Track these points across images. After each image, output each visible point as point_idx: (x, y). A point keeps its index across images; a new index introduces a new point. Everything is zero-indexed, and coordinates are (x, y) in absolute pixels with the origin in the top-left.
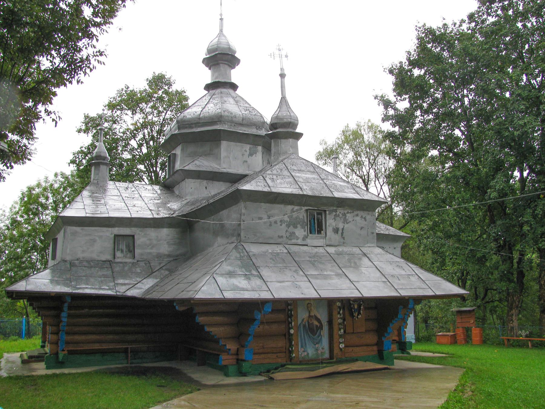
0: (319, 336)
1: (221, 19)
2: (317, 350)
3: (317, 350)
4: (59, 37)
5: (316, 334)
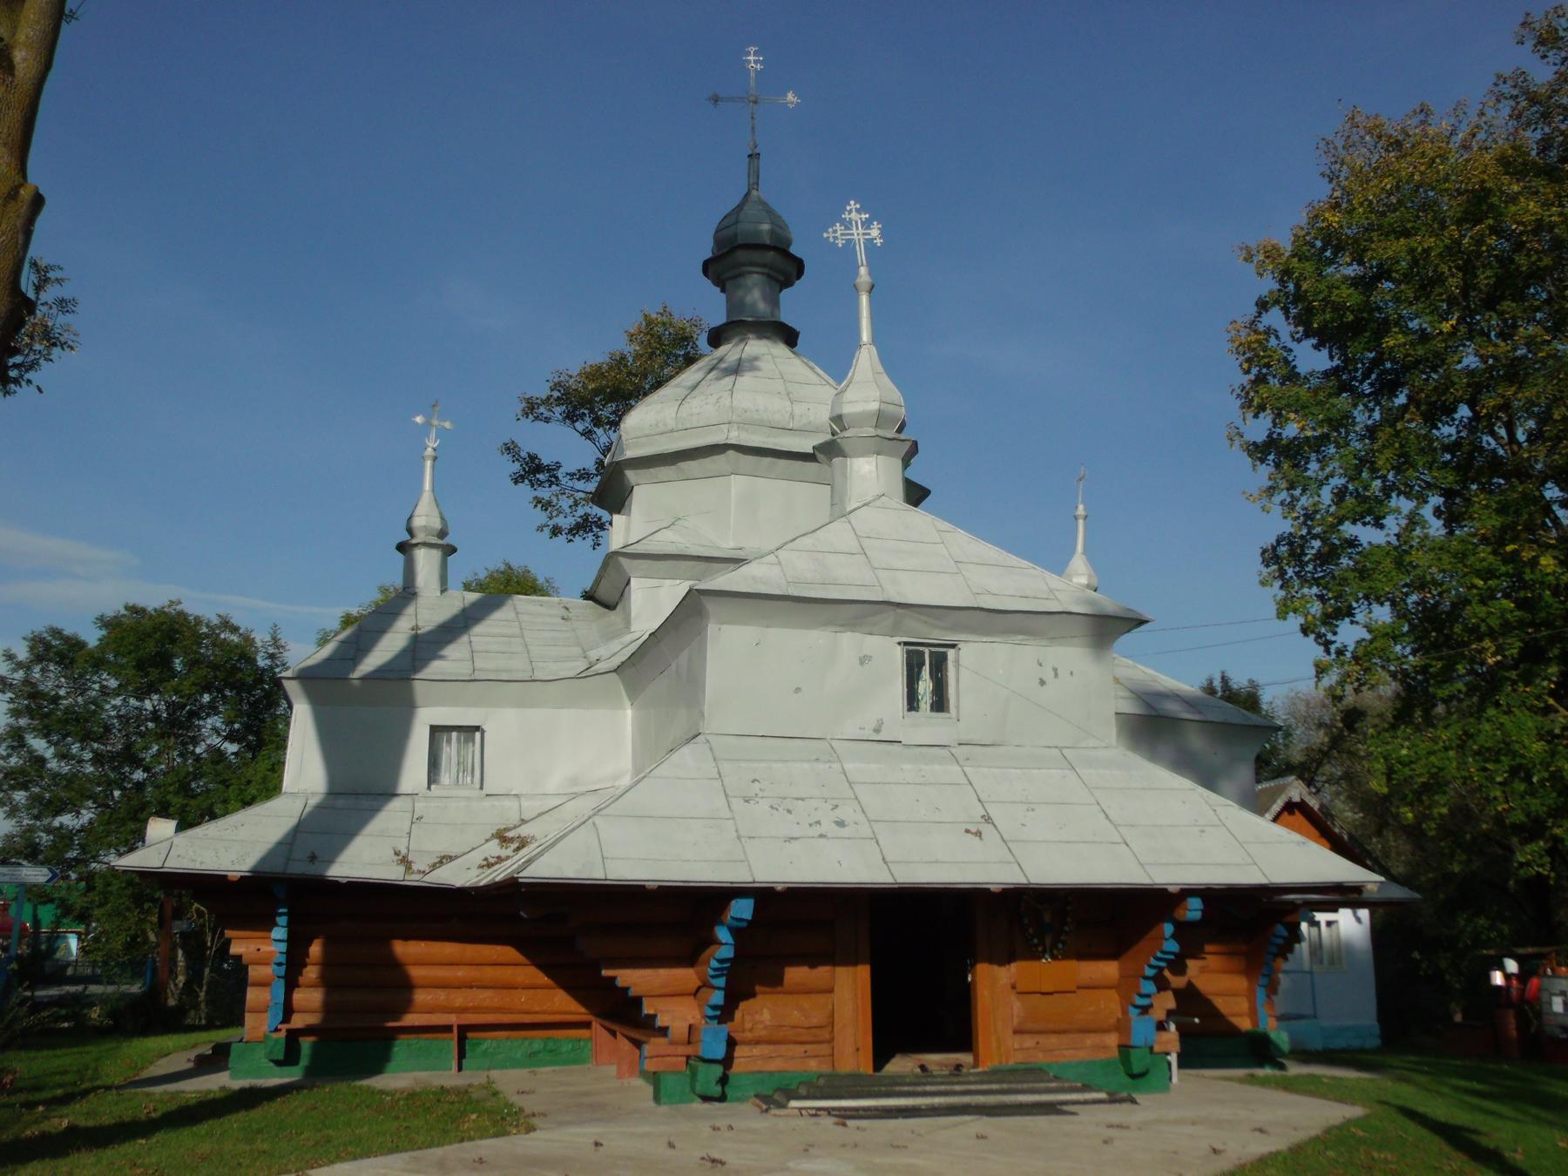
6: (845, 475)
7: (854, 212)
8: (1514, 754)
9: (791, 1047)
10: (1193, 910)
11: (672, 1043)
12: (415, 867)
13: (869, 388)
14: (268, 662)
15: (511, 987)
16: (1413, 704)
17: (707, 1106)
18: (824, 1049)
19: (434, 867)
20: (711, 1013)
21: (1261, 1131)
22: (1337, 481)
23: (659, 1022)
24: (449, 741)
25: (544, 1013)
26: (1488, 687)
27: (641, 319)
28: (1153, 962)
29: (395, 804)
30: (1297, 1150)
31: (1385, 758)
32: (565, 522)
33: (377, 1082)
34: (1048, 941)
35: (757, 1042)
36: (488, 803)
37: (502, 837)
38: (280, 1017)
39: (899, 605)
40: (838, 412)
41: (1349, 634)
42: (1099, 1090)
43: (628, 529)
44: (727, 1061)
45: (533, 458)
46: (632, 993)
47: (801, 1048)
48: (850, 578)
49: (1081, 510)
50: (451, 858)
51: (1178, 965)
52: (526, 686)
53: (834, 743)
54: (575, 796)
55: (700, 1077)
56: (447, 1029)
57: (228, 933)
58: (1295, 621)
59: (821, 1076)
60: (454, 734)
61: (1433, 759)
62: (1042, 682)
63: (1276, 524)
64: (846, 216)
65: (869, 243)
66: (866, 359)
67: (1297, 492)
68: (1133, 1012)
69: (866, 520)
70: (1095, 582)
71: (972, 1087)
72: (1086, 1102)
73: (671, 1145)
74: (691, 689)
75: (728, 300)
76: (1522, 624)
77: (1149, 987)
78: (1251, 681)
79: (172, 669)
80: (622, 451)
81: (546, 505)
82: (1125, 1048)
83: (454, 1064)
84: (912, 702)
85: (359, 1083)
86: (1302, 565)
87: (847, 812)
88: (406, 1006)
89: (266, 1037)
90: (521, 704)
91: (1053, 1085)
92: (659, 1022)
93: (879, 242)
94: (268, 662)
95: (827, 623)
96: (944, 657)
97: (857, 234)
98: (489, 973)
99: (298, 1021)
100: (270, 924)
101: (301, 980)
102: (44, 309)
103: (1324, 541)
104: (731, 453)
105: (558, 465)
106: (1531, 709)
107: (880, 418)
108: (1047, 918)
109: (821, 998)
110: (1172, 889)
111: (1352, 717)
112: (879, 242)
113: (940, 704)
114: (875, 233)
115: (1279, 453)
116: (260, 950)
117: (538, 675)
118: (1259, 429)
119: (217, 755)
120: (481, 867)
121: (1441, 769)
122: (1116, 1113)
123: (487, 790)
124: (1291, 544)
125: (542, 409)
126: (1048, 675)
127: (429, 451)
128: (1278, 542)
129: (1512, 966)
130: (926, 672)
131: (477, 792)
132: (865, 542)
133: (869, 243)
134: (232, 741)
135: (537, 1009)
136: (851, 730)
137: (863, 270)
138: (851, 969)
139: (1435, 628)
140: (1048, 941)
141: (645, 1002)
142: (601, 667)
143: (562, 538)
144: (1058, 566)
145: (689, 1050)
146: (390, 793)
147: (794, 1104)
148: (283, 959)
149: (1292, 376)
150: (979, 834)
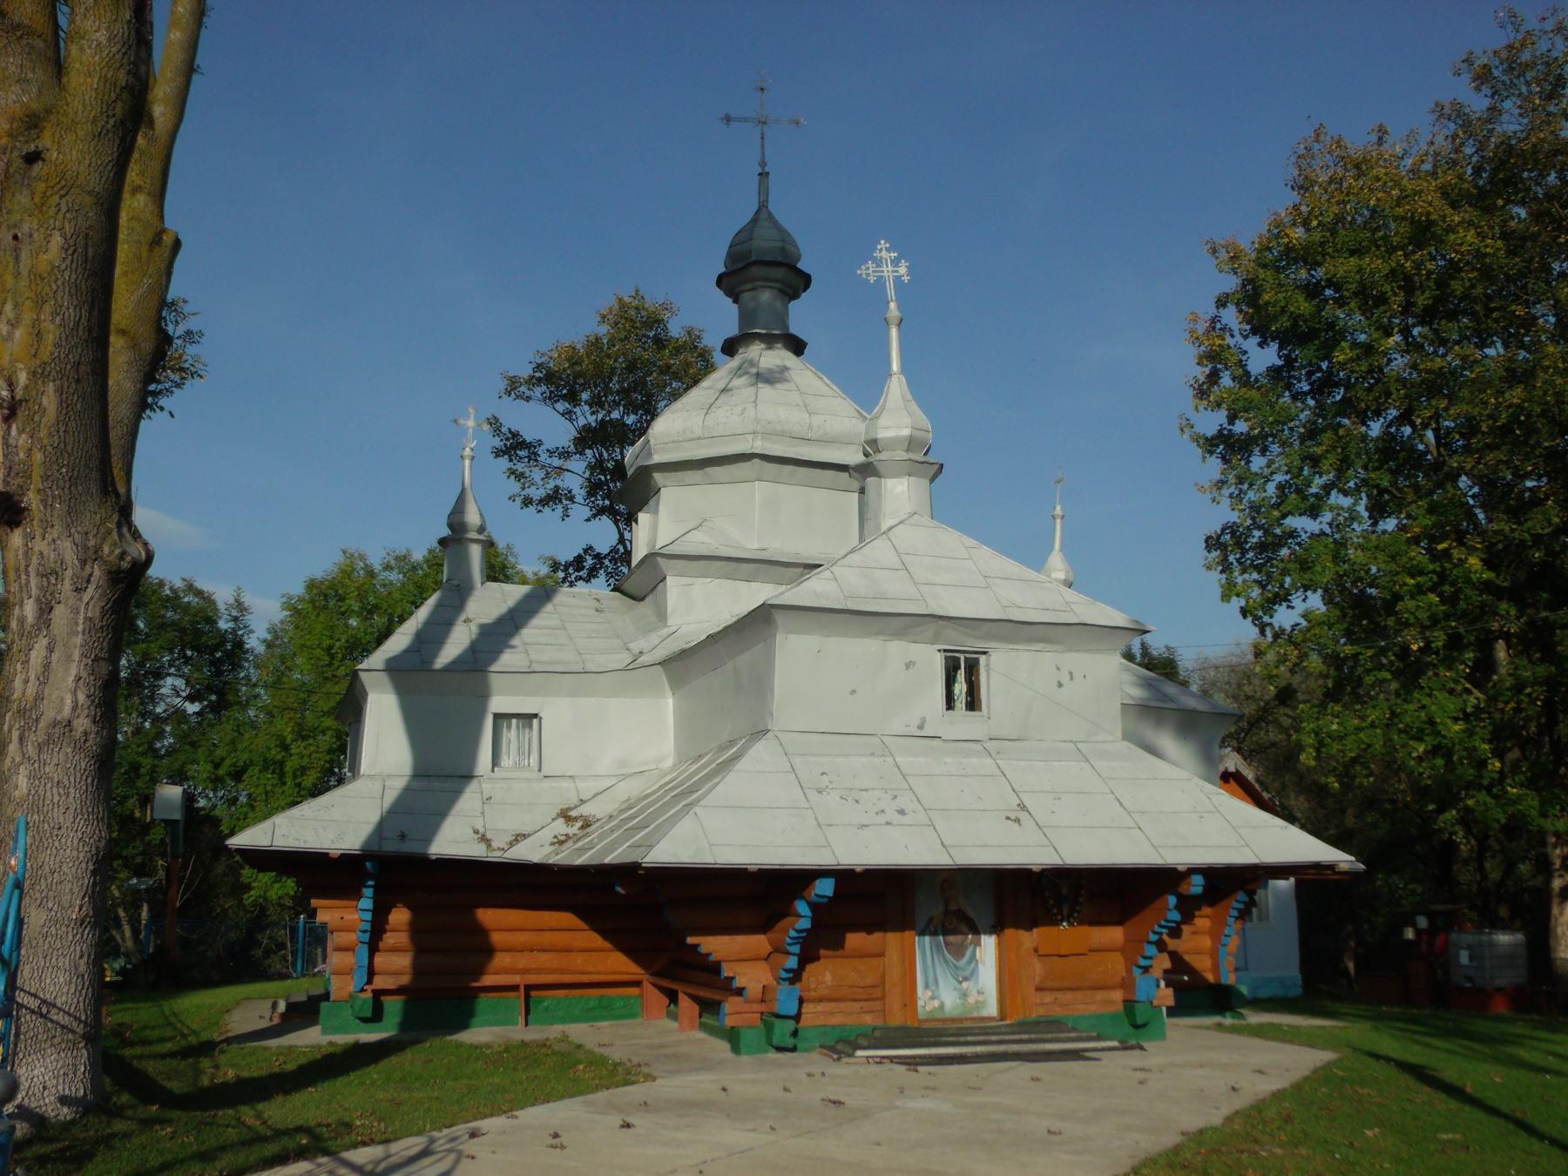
0: (969, 962)
1: (764, 175)
2: (965, 995)
3: (965, 995)
4: (289, 903)
5: (963, 955)
6: (879, 494)
7: (884, 251)
8: (1438, 734)
9: (849, 1004)
10: (1196, 885)
11: (747, 1001)
12: (495, 845)
13: (898, 417)
14: (231, 625)
15: (568, 950)
16: (1344, 686)
17: (780, 1056)
18: (877, 1005)
19: (511, 844)
20: (784, 975)
21: (1260, 1072)
22: (1280, 478)
23: (737, 984)
24: (509, 727)
25: (599, 973)
26: (1410, 671)
27: (614, 303)
28: (1157, 929)
29: (473, 787)
30: (1297, 1087)
31: (1317, 734)
32: (537, 493)
33: (465, 1037)
34: (1065, 912)
35: (820, 1000)
36: (547, 784)
37: (565, 815)
38: (365, 979)
39: (941, 617)
40: (872, 436)
41: (1285, 617)
42: (1110, 1039)
43: (654, 528)
44: (797, 1018)
45: (515, 435)
46: (711, 958)
47: (858, 1005)
48: (898, 595)
49: (1058, 510)
50: (525, 836)
51: (1175, 932)
52: (577, 678)
53: (885, 739)
54: (625, 777)
55: (777, 1031)
56: (515, 988)
57: (314, 902)
58: (1237, 603)
59: (874, 1029)
60: (514, 721)
61: (1362, 735)
62: (1060, 685)
63: (1223, 514)
64: (876, 254)
65: (898, 279)
66: (897, 387)
67: (1245, 486)
68: (1137, 971)
69: (904, 536)
70: (1071, 579)
71: (1006, 1037)
72: (1103, 1049)
73: (785, 1089)
74: (759, 686)
75: (740, 309)
76: (1447, 616)
77: (1151, 950)
78: (1168, 648)
79: (135, 629)
80: (649, 454)
81: (519, 476)
82: (1129, 1004)
83: (521, 1020)
84: (950, 703)
85: (449, 1038)
86: (1244, 552)
87: (905, 801)
88: (479, 972)
89: (351, 996)
90: (573, 694)
91: (1073, 1035)
92: (737, 984)
93: (906, 279)
94: (231, 625)
95: (878, 634)
96: (977, 660)
97: (887, 270)
98: (547, 938)
99: (380, 982)
100: (358, 895)
101: (381, 945)
102: (179, 342)
103: (1266, 532)
104: (756, 461)
105: (540, 443)
106: (1451, 692)
107: (912, 443)
108: (1065, 891)
109: (874, 962)
110: (1180, 868)
111: (1286, 695)
112: (906, 279)
113: (973, 704)
114: (903, 270)
115: (1227, 446)
116: (344, 918)
117: (590, 667)
118: (1211, 422)
119: (179, 716)
120: (553, 844)
121: (1369, 746)
122: (1132, 1058)
123: (545, 771)
124: (1233, 533)
125: (523, 389)
126: (1065, 679)
127: (467, 451)
128: (1223, 530)
129: (1422, 922)
130: (961, 676)
131: (535, 775)
132: (905, 557)
133: (898, 279)
134: (192, 702)
135: (591, 969)
136: (897, 726)
137: (893, 305)
138: (899, 934)
139: (1360, 610)
140: (1065, 912)
141: (724, 966)
142: (644, 659)
143: (532, 509)
144: (1037, 562)
145: (763, 1008)
146: (468, 777)
147: (859, 1053)
148: (368, 926)
149: (1244, 379)
150: (1017, 820)
